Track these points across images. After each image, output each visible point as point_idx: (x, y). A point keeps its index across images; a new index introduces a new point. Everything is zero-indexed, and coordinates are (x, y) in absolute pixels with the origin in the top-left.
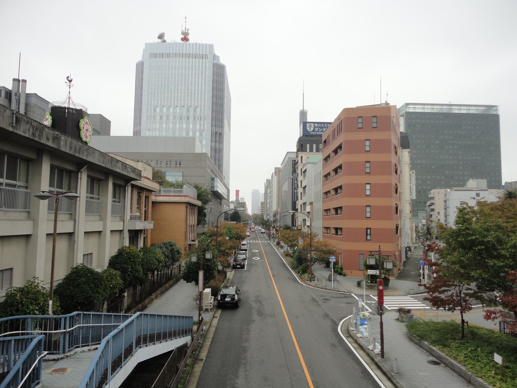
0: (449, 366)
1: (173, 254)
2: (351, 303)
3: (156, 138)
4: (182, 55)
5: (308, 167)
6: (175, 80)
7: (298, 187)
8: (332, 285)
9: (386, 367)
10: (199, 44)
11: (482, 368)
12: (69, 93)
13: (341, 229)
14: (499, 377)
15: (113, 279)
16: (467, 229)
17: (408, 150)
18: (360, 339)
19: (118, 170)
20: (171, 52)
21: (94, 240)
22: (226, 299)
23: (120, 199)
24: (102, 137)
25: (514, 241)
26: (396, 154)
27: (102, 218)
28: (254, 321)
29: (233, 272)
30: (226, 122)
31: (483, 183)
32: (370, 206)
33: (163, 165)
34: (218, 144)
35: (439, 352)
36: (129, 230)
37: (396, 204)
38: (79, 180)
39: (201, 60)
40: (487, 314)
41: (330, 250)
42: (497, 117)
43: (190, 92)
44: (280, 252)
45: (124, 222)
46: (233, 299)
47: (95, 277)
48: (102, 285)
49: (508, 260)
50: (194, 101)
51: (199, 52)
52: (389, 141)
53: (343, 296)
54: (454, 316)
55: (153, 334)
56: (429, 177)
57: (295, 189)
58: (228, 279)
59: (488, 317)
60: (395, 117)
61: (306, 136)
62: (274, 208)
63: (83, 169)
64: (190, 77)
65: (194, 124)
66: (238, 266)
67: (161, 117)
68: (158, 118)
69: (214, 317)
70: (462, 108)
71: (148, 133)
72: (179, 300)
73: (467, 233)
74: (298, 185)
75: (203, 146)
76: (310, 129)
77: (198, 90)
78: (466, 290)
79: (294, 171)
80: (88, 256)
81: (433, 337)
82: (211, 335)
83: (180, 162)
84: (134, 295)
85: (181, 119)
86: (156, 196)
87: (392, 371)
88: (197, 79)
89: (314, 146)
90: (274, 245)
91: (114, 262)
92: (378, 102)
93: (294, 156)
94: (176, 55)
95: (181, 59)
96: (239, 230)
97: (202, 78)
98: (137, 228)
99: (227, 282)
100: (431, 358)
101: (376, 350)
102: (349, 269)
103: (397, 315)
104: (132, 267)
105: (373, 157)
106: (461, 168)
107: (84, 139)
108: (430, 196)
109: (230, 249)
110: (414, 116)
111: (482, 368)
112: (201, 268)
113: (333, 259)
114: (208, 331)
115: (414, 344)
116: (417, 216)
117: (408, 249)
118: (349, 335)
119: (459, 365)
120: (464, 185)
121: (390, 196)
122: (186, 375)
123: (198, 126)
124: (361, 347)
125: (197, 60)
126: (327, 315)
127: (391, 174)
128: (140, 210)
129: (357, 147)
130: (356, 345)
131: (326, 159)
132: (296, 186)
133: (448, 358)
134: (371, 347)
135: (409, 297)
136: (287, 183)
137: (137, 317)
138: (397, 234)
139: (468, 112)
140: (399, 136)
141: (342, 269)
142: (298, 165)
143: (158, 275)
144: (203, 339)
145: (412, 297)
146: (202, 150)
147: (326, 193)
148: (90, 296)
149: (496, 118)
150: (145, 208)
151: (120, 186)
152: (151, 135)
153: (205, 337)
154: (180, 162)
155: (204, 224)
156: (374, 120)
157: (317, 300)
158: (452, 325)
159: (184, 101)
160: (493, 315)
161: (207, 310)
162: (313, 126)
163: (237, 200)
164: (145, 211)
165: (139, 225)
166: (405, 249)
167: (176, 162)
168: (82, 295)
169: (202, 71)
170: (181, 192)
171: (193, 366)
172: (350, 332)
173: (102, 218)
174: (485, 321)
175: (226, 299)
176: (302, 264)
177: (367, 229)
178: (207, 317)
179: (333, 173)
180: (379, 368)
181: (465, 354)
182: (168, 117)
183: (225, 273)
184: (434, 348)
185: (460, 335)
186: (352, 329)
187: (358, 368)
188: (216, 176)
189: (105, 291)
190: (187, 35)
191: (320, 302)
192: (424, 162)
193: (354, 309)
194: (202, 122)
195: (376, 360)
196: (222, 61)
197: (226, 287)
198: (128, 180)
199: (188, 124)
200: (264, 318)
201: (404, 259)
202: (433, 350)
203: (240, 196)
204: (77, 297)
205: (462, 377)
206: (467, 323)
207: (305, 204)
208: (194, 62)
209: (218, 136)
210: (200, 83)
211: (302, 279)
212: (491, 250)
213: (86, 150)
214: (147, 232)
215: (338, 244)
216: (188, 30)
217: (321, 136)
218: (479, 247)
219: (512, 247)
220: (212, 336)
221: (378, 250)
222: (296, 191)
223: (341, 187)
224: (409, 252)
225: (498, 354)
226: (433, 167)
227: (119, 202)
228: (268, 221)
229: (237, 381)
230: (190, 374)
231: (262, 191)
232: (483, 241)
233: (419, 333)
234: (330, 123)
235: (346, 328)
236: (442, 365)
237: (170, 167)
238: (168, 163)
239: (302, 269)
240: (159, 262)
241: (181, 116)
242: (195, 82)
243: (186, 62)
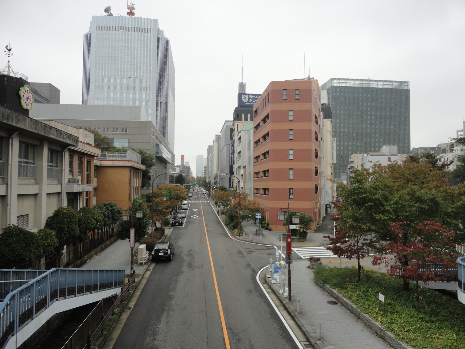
0: (345, 305)
1: (112, 213)
2: (272, 254)
3: (103, 106)
4: (128, 29)
5: (242, 134)
6: (121, 52)
7: (234, 152)
8: (258, 238)
9: (291, 308)
10: (145, 19)
11: (369, 306)
12: (9, 61)
13: (268, 189)
14: (382, 312)
15: (48, 238)
16: (361, 188)
17: (330, 120)
18: (274, 285)
19: (52, 137)
20: (117, 25)
21: (29, 202)
22: (160, 254)
23: (57, 164)
24: (50, 105)
25: (396, 199)
26: (317, 124)
27: (38, 182)
28: (183, 272)
29: (172, 229)
30: (170, 93)
31: (395, 148)
32: (292, 169)
33: (110, 132)
34: (162, 113)
35: (337, 293)
36: (67, 193)
37: (316, 167)
38: (10, 145)
39: (146, 34)
40: (374, 260)
41: (257, 208)
42: (408, 91)
43: (136, 63)
44: (215, 209)
45: (62, 185)
46: (166, 253)
47: (28, 236)
48: (33, 243)
49: (392, 214)
50: (140, 72)
51: (144, 26)
52: (310, 111)
53: (266, 248)
54: (352, 263)
55: (73, 288)
56: (350, 144)
57: (232, 154)
58: (166, 236)
59: (375, 263)
60: (316, 90)
61: (242, 106)
62: (215, 171)
63: (15, 135)
64: (136, 49)
65: (141, 94)
66: (177, 224)
67: (109, 87)
68: (106, 87)
69: (147, 270)
70: (379, 83)
71: (96, 102)
72: (116, 256)
73: (359, 192)
74: (234, 151)
75: (148, 115)
76: (245, 100)
77: (144, 62)
78: (363, 240)
79: (231, 138)
80: (23, 217)
81: (335, 281)
82: (142, 286)
83: (126, 129)
84: (75, 251)
85: (128, 89)
86: (101, 161)
87: (296, 311)
88: (142, 52)
89: (249, 116)
90: (213, 205)
91: (50, 223)
92: (299, 78)
93: (231, 124)
94: (122, 28)
95: (127, 33)
96: (179, 192)
97: (147, 51)
98: (75, 191)
99: (165, 238)
100: (331, 299)
101: (285, 294)
102: (275, 224)
103: (308, 263)
104: (68, 227)
105: (296, 126)
106: (377, 136)
107: (25, 107)
108: (350, 160)
109: (167, 209)
110: (338, 90)
111: (369, 306)
112: (133, 226)
113: (258, 216)
114: (139, 283)
115: (319, 288)
116: (340, 177)
117: (328, 206)
118: (265, 281)
119: (351, 304)
120: (379, 150)
121: (310, 160)
122: (112, 323)
123: (144, 96)
124: (274, 292)
125: (143, 34)
126: (249, 265)
127: (310, 141)
128: (82, 173)
129: (282, 116)
130: (269, 290)
131: (256, 127)
132: (232, 152)
133: (344, 298)
134: (281, 292)
135: (322, 247)
136: (225, 149)
137: (52, 273)
138: (316, 193)
139: (384, 87)
140: (320, 107)
141: (268, 225)
142: (234, 132)
143: (98, 233)
144: (134, 290)
145: (324, 247)
146: (148, 118)
147: (257, 158)
148: (22, 254)
149: (407, 92)
150: (87, 171)
151: (57, 152)
152: (99, 103)
153: (136, 288)
154: (126, 129)
155: (148, 186)
156: (297, 92)
157: (243, 252)
158: (352, 271)
159: (131, 72)
160: (379, 261)
161: (141, 264)
162: (248, 98)
163: (182, 164)
164: (88, 175)
165: (76, 188)
166: (325, 206)
167: (123, 129)
168: (13, 254)
169: (147, 44)
170: (125, 157)
171: (120, 315)
172: (266, 279)
173: (38, 182)
174: (373, 266)
175: (160, 254)
176: (234, 221)
177: (290, 189)
178: (139, 270)
179: (262, 140)
180: (286, 309)
181: (358, 295)
182: (115, 87)
183: (163, 231)
184: (334, 290)
185: (357, 278)
186: (268, 276)
187: (267, 309)
188: (161, 143)
189: (37, 249)
190: (132, 10)
191: (245, 254)
192: (346, 130)
193: (271, 259)
194: (148, 92)
195: (284, 302)
196: (167, 35)
197: (163, 243)
198: (64, 146)
199: (134, 94)
200: (193, 269)
201: (323, 214)
202: (333, 292)
203: (185, 161)
204: (8, 255)
205: (353, 313)
206: (363, 268)
207: (239, 167)
208: (139, 35)
209: (163, 106)
210: (142, 56)
211: (232, 234)
212: (378, 206)
213: (16, 117)
214: (90, 194)
215: (265, 203)
216: (134, 5)
217: (252, 106)
218: (369, 203)
219: (394, 204)
220: (142, 287)
221: (287, 207)
222: (232, 156)
223: (268, 152)
224: (329, 209)
225: (382, 294)
226: (354, 135)
227: (57, 167)
228: (209, 183)
229: (159, 326)
230: (117, 321)
231: (205, 156)
232: (372, 199)
233: (324, 277)
234: (260, 95)
235: (264, 276)
236: (339, 304)
237: (117, 134)
238: (115, 130)
239: (233, 226)
240: (97, 221)
241: (128, 87)
242: (141, 54)
243: (131, 35)
